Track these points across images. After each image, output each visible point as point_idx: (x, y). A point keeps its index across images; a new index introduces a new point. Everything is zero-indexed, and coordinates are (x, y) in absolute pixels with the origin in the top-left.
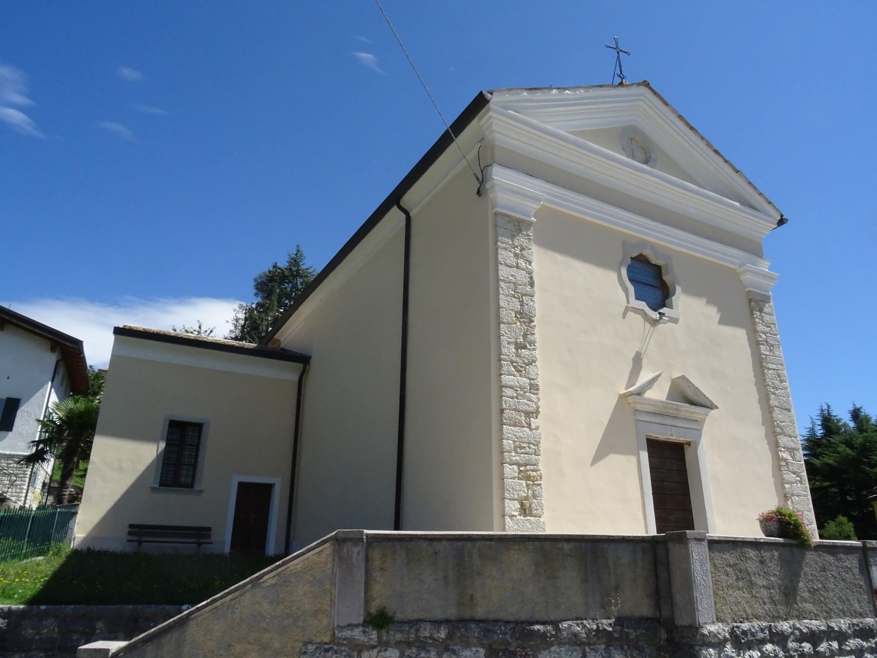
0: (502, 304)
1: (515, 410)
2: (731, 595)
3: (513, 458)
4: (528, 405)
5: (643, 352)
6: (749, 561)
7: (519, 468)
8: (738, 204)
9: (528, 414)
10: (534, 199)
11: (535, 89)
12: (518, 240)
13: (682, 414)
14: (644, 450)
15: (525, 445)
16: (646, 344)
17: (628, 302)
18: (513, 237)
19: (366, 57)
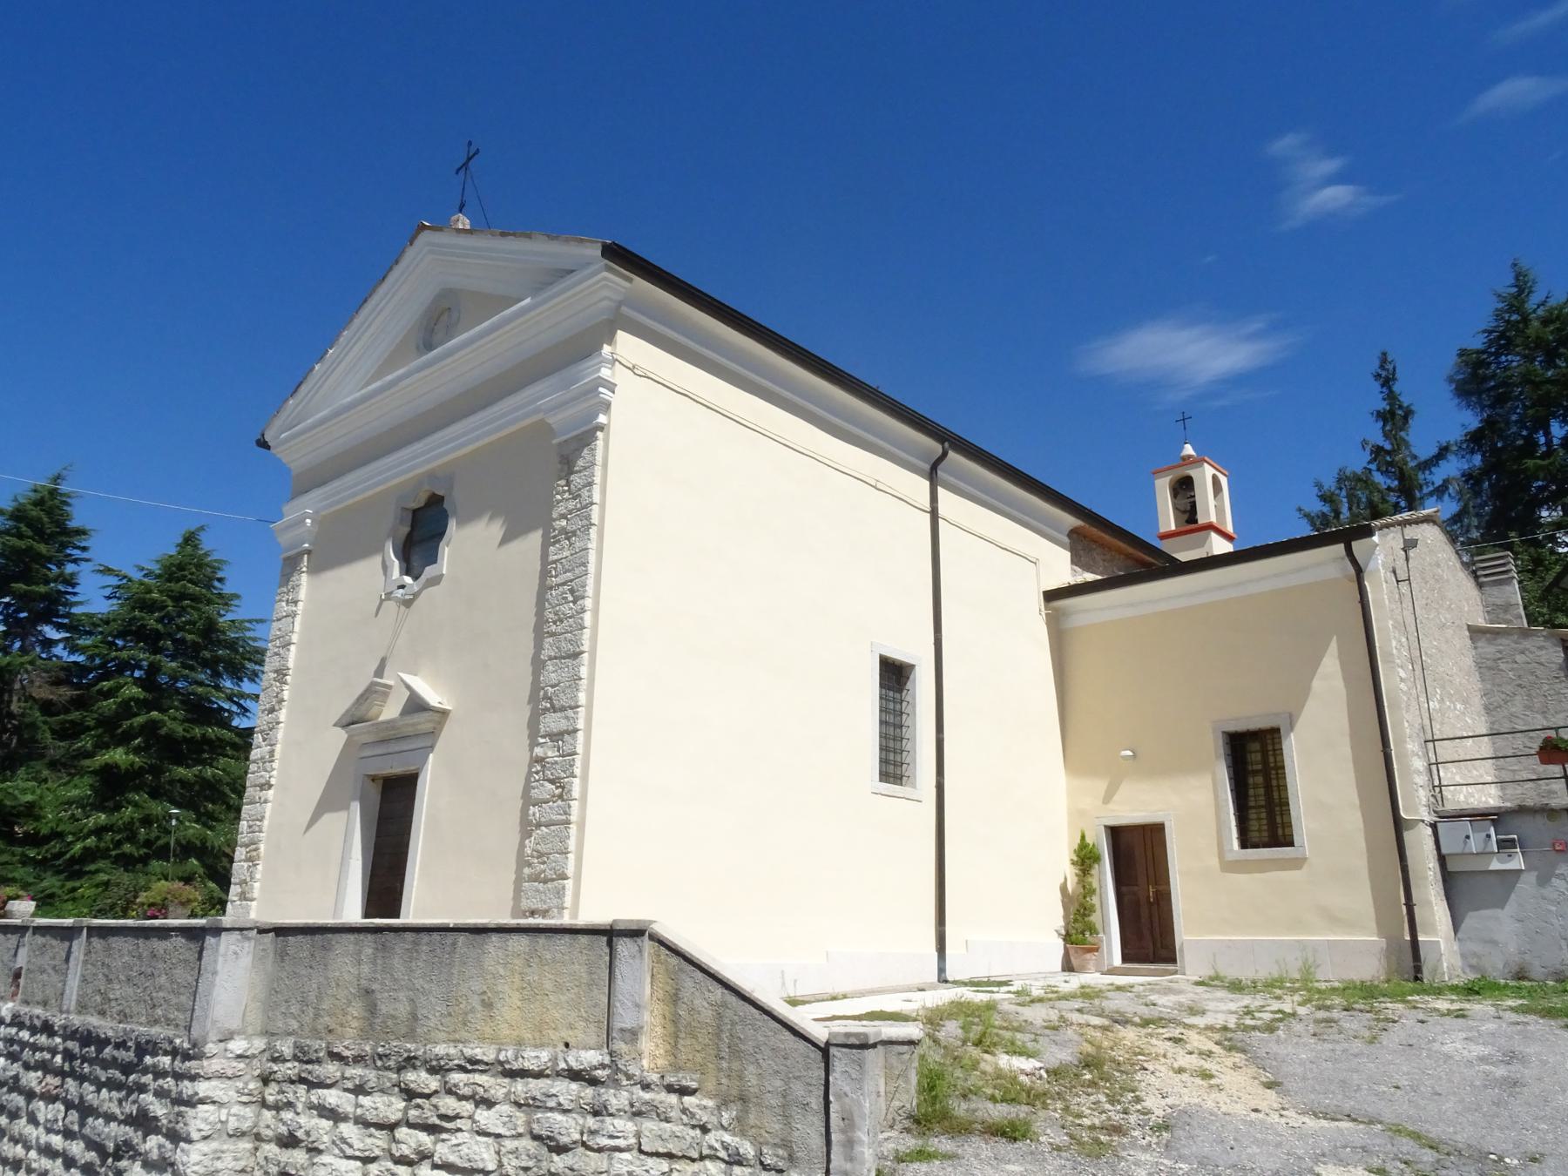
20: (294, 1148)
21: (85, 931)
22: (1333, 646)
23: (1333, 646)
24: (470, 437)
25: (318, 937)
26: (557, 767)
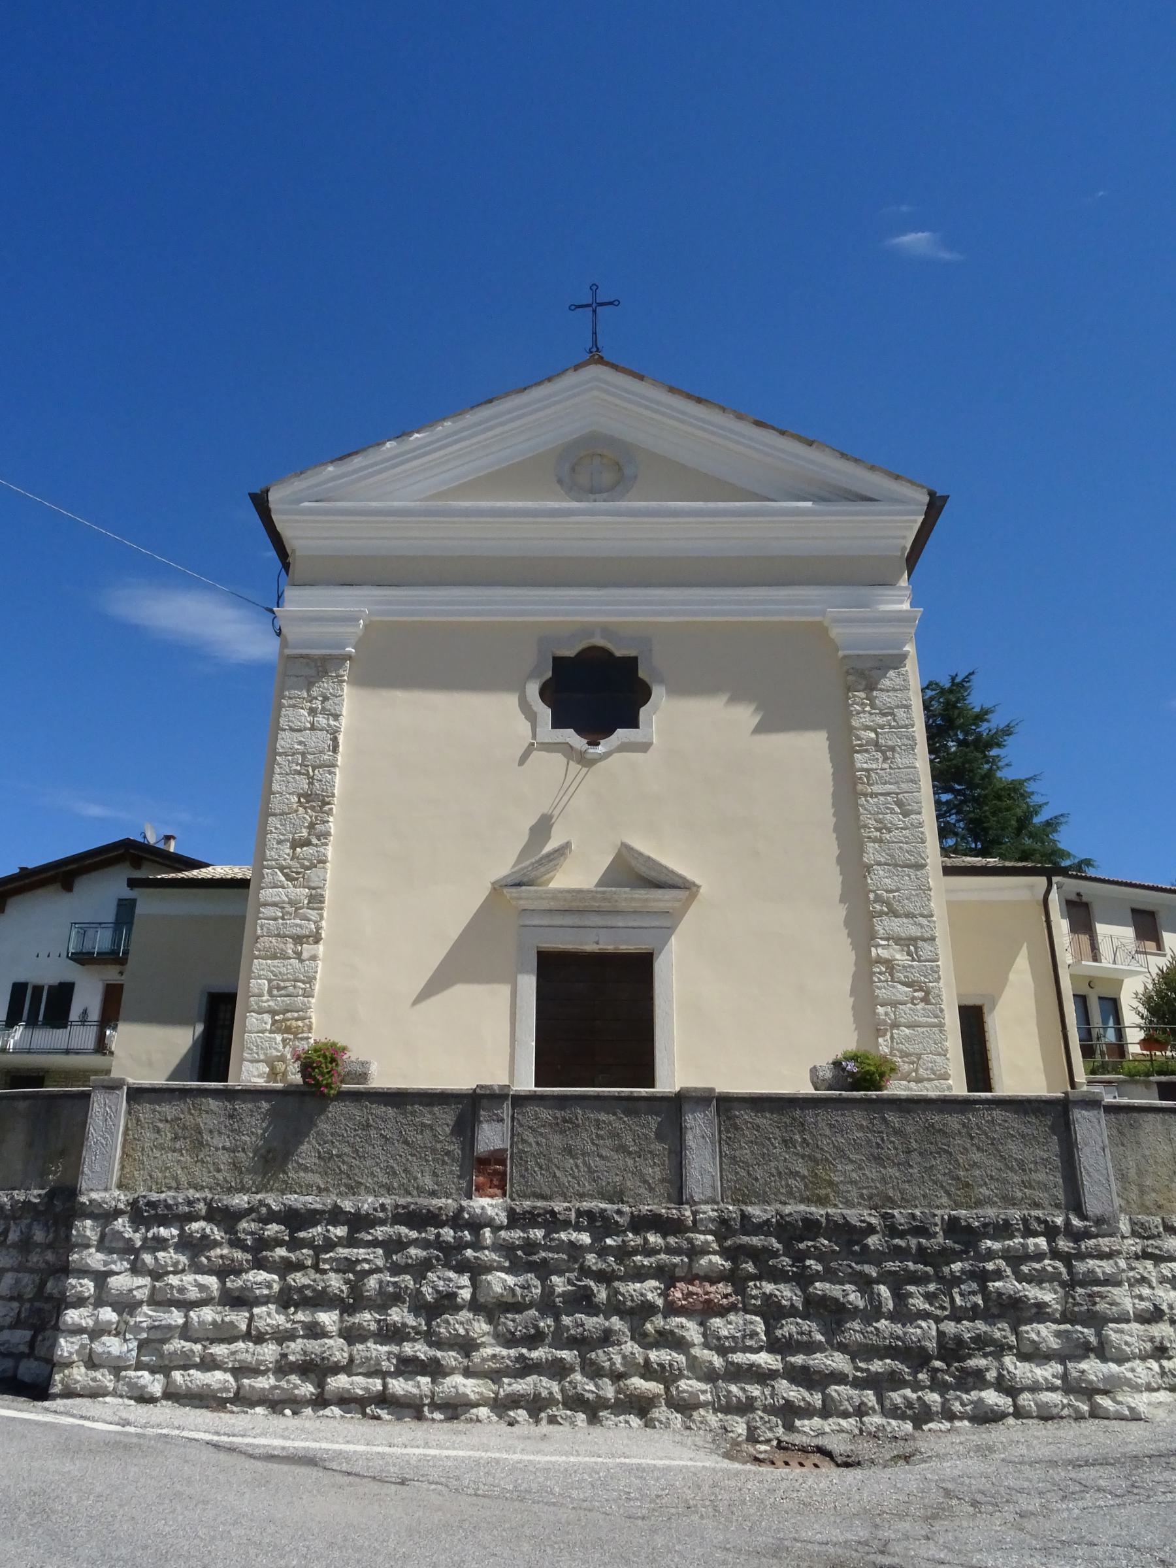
0: (275, 787)
1: (278, 935)
2: (155, 1158)
3: (265, 1004)
4: (300, 926)
5: (556, 813)
6: (204, 1115)
7: (273, 1017)
8: (809, 504)
9: (299, 940)
10: (352, 619)
11: (349, 455)
12: (319, 687)
13: (623, 905)
14: (528, 972)
15: (288, 984)
16: (566, 799)
17: (534, 736)
18: (309, 686)
19: (915, 241)
20: (1157, 1322)
21: (715, 1102)
22: (1024, 950)
23: (1024, 950)
24: (724, 607)
25: (1122, 1116)
26: (913, 971)
